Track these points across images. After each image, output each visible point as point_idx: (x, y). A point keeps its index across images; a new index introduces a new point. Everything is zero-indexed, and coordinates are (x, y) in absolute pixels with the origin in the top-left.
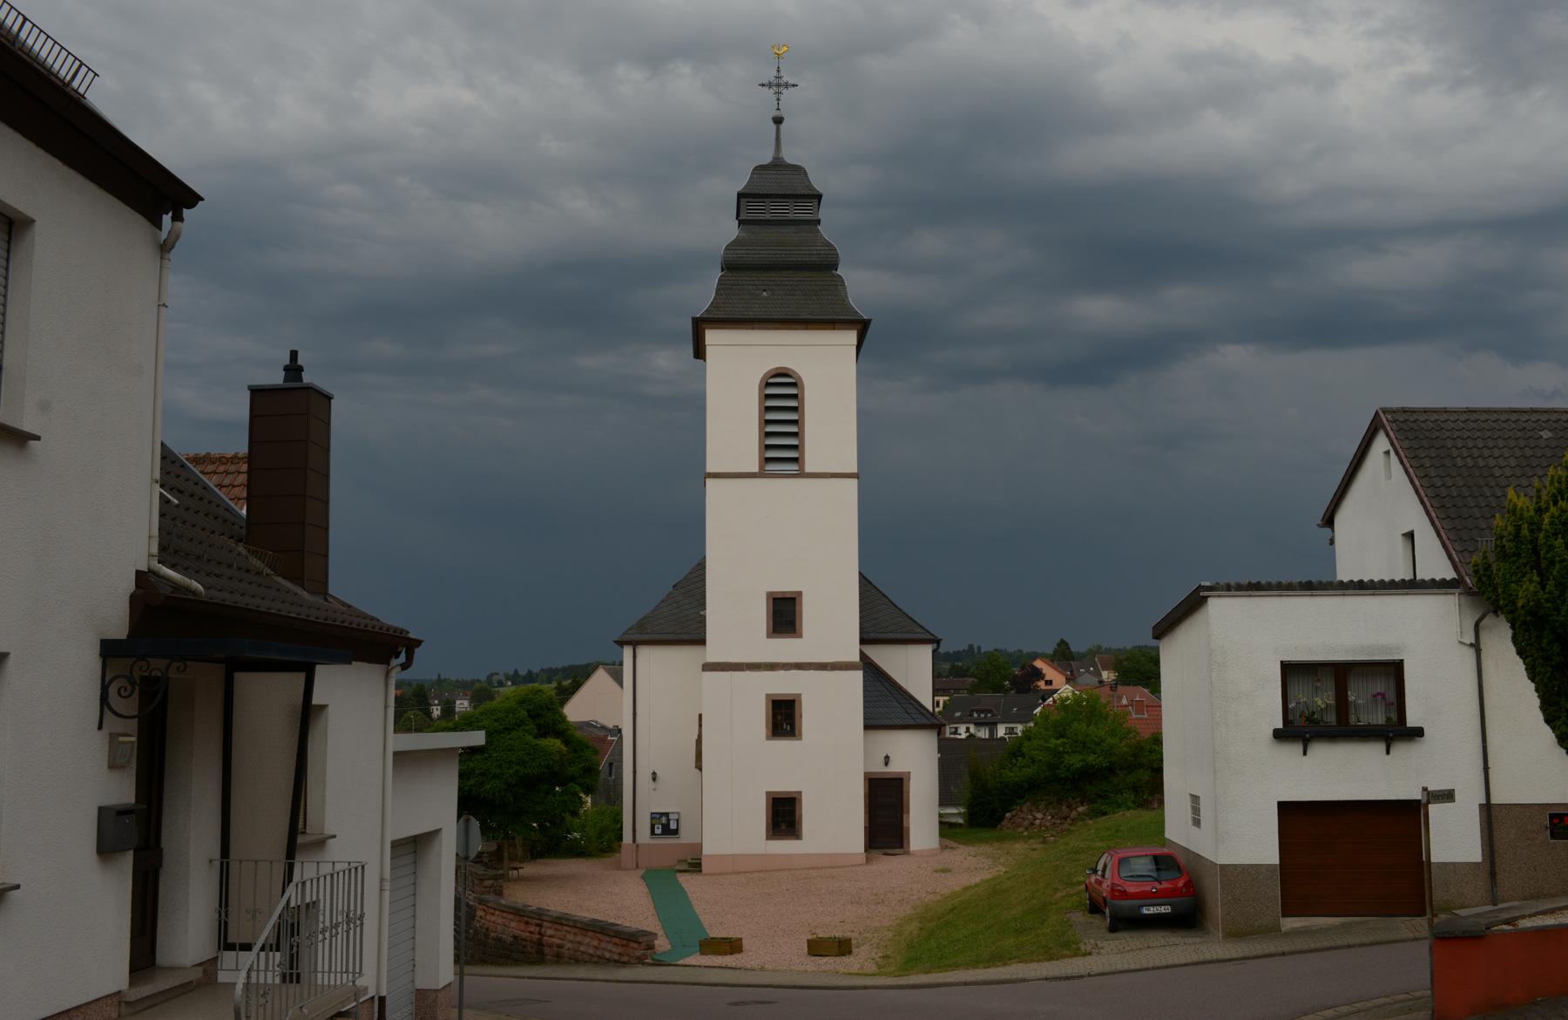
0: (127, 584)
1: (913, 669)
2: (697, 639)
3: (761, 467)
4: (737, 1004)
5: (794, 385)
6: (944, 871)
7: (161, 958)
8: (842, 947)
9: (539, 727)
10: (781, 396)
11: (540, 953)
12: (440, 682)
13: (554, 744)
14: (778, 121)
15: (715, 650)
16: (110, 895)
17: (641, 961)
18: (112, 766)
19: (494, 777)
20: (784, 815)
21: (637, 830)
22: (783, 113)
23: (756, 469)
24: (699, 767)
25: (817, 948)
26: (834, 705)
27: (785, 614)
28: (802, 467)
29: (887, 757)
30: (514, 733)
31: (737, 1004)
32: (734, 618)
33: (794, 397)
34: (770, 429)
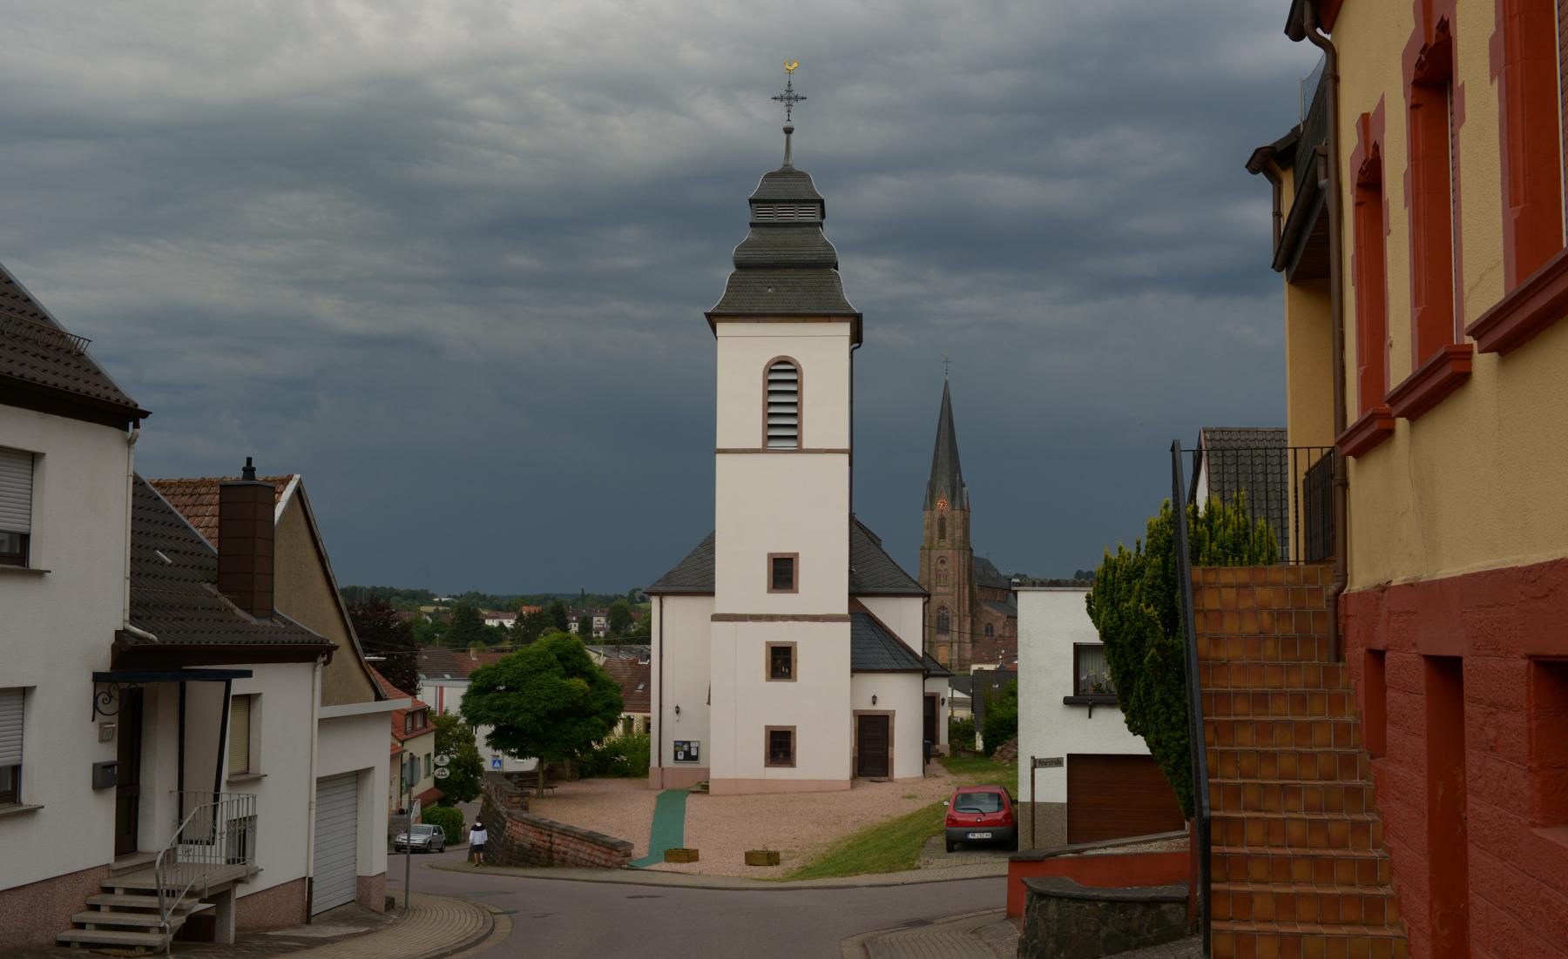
0: (110, 639)
1: (905, 619)
3: (764, 444)
4: (911, 924)
5: (794, 371)
6: (910, 797)
7: (140, 847)
8: (772, 859)
9: (566, 668)
10: (783, 380)
11: (551, 857)
13: (579, 683)
14: (788, 131)
15: (723, 601)
16: (102, 813)
17: (619, 866)
18: (102, 740)
20: (780, 746)
21: (662, 757)
22: (794, 123)
23: (760, 446)
25: (752, 859)
26: (826, 651)
27: (783, 573)
28: (800, 444)
29: (874, 697)
30: (545, 674)
31: (911, 924)
34: (773, 410)
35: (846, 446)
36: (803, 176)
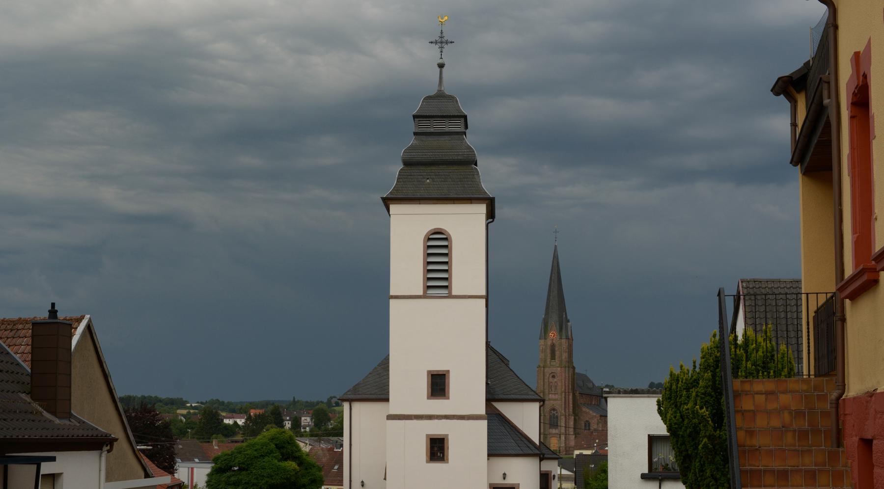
1: (526, 418)
2: (383, 397)
3: (425, 292)
5: (446, 239)
9: (282, 454)
10: (438, 245)
12: (294, 403)
13: (292, 465)
14: (441, 66)
15: (395, 406)
19: (253, 485)
22: (445, 60)
23: (421, 293)
24: (385, 479)
27: (438, 384)
28: (450, 292)
29: (505, 474)
30: (266, 459)
32: (407, 385)
33: (446, 247)
34: (431, 267)
35: (484, 293)
36: (451, 98)
